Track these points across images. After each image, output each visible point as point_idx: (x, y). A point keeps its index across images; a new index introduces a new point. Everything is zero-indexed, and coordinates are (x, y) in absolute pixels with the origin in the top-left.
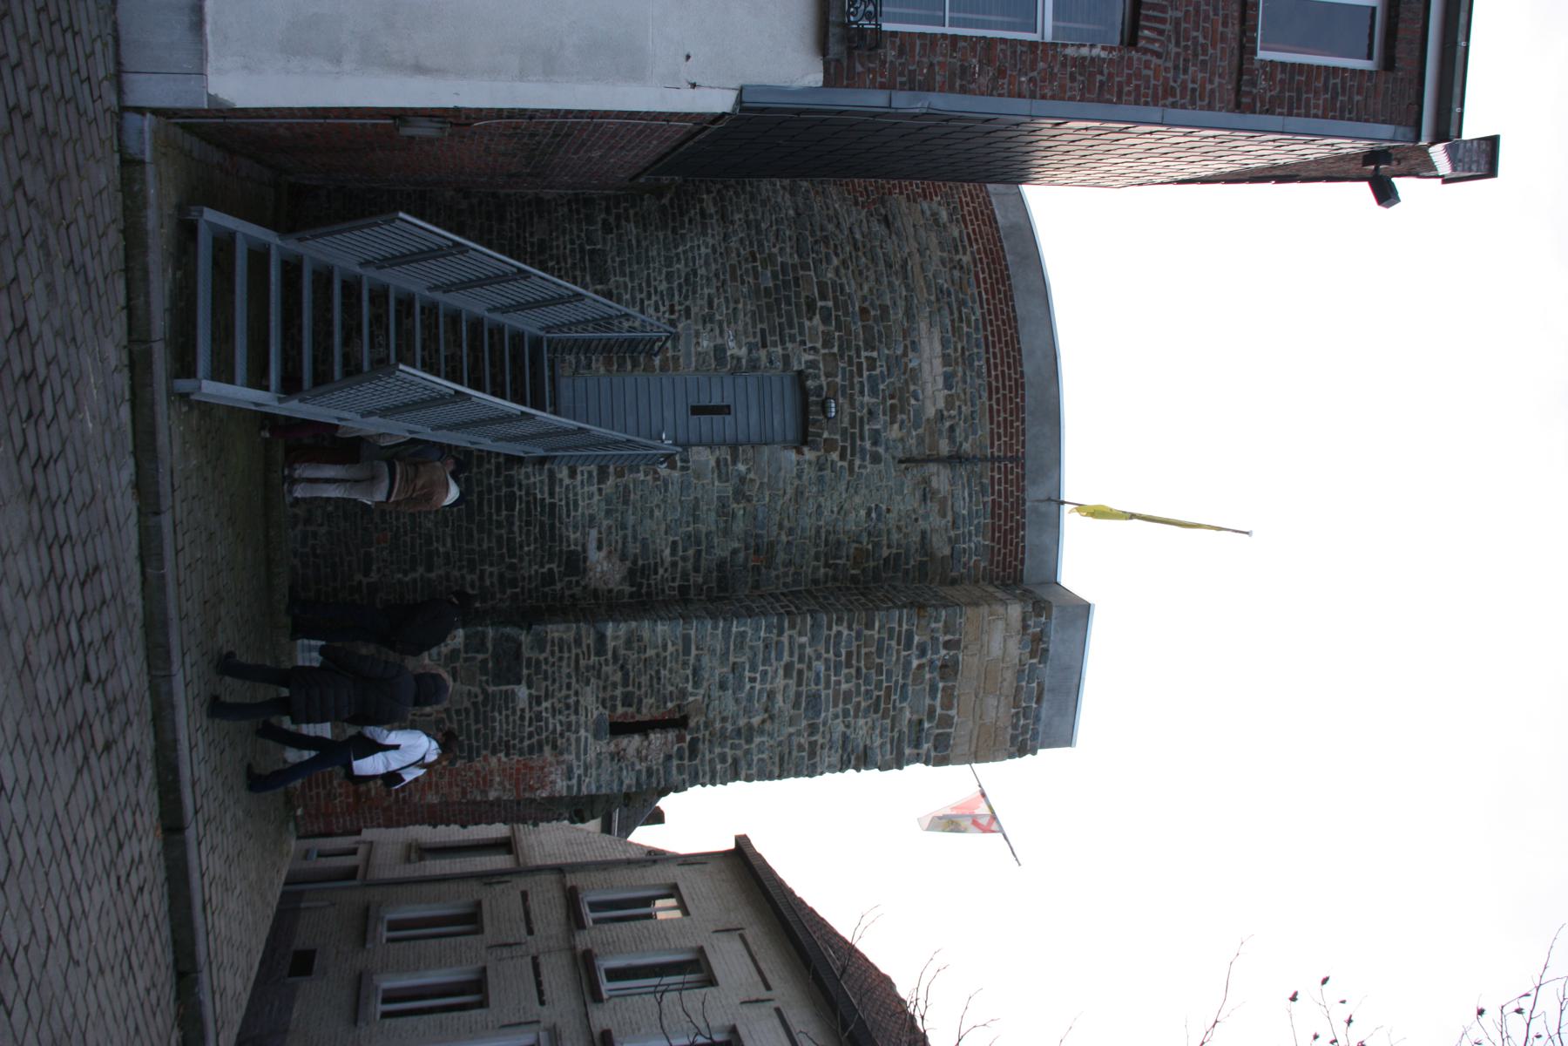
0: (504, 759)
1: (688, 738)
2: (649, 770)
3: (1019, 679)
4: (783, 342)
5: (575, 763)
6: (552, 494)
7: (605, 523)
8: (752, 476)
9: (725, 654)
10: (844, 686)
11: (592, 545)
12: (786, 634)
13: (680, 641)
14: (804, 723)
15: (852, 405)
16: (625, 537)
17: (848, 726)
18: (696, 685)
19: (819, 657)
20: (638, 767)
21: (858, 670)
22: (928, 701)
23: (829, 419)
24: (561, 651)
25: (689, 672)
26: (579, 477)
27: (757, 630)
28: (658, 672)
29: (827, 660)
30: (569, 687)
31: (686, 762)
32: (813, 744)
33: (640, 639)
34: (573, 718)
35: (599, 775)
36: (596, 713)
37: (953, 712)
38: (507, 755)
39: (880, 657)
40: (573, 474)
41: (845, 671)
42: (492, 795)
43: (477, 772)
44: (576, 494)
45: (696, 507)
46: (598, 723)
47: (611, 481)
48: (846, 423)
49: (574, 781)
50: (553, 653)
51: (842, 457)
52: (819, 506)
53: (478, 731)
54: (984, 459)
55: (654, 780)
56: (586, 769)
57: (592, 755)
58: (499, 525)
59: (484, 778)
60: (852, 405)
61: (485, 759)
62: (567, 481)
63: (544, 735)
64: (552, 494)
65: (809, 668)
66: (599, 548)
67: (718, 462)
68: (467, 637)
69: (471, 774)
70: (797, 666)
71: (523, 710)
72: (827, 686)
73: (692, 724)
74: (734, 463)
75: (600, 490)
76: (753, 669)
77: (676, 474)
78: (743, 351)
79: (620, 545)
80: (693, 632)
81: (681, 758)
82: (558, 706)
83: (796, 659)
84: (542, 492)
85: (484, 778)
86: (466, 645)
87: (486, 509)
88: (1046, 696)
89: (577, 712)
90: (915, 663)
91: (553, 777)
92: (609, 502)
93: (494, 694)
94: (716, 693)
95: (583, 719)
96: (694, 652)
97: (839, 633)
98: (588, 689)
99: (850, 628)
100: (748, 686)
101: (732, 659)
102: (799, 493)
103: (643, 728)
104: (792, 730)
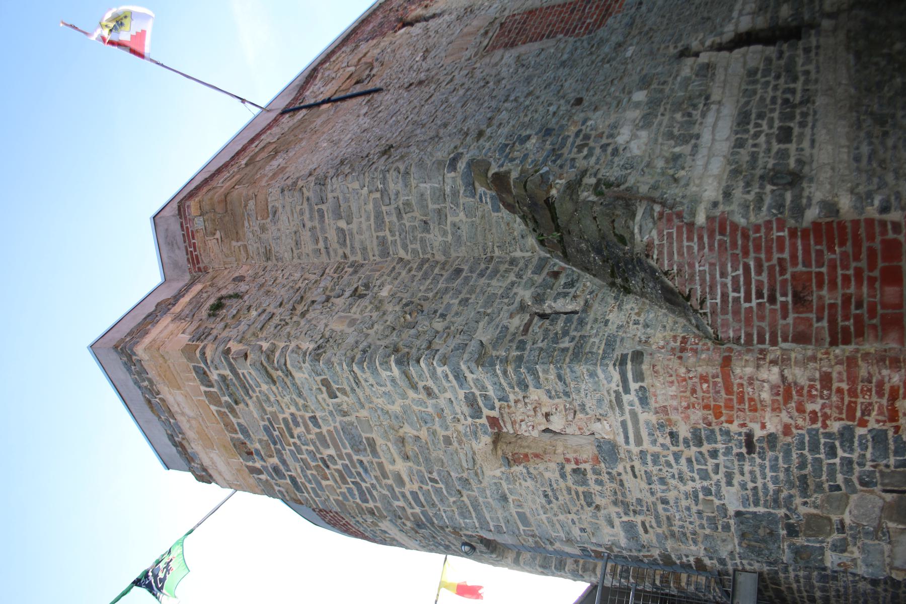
49: (634, 386)
69: (810, 407)
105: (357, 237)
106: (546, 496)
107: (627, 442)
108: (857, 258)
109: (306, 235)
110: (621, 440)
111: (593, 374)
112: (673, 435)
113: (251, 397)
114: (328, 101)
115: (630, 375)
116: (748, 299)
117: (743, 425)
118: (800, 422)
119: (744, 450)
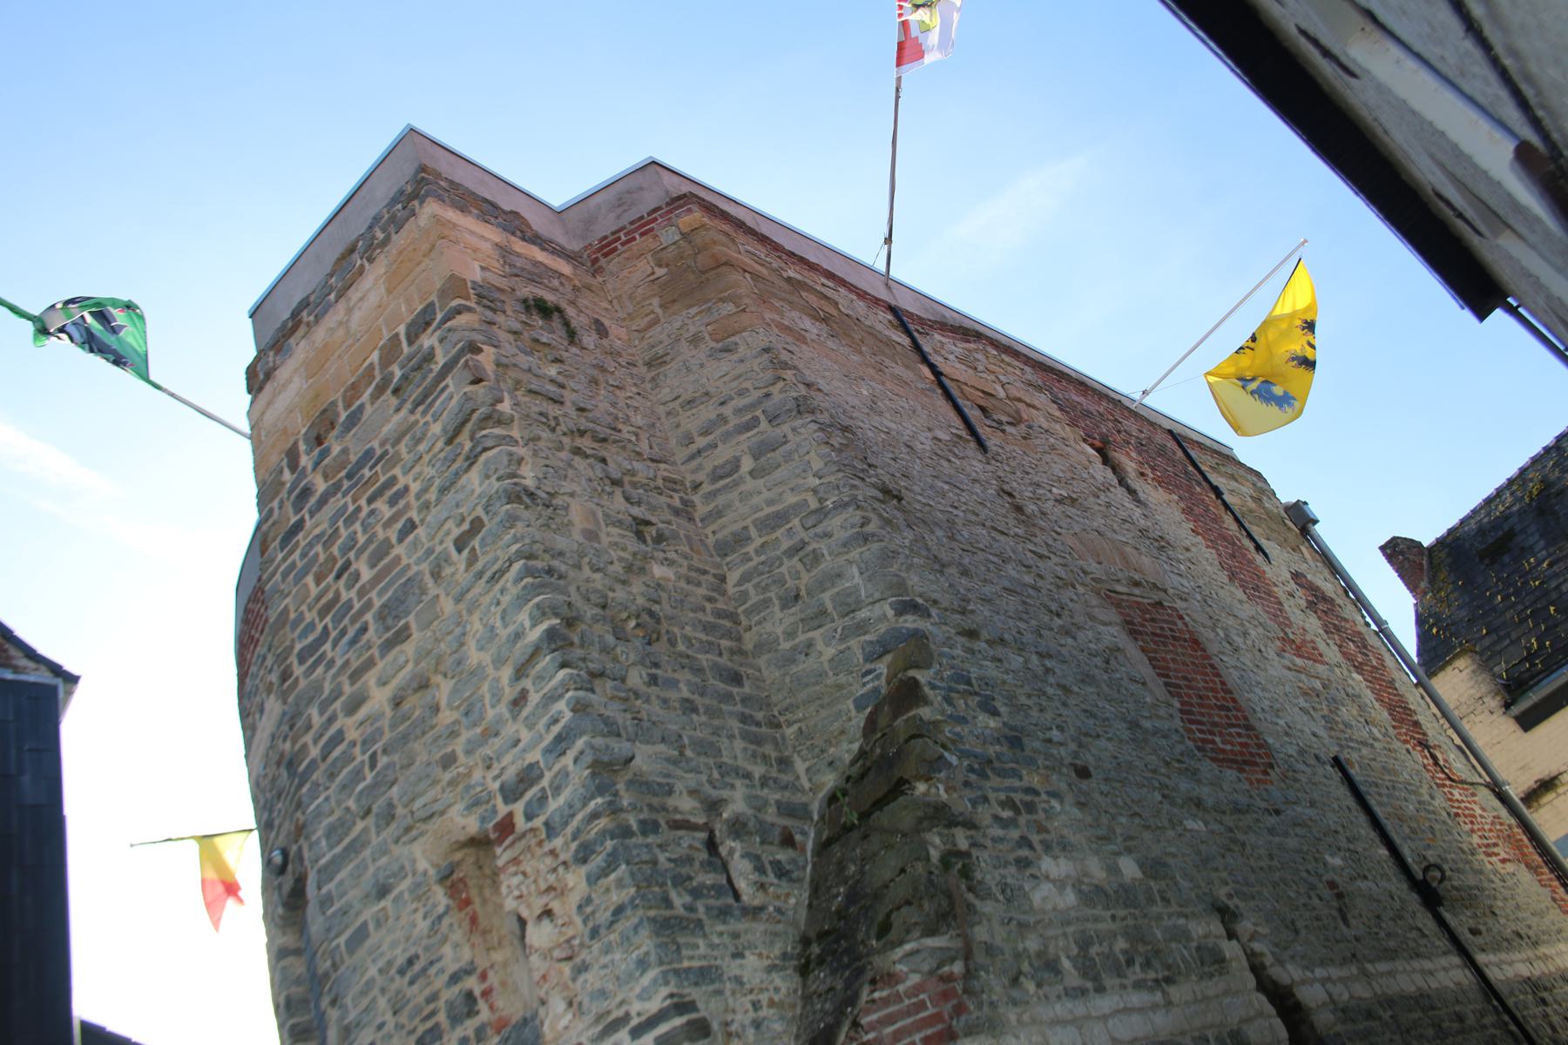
105: (734, 495)
109: (708, 412)
111: (643, 964)
113: (412, 412)
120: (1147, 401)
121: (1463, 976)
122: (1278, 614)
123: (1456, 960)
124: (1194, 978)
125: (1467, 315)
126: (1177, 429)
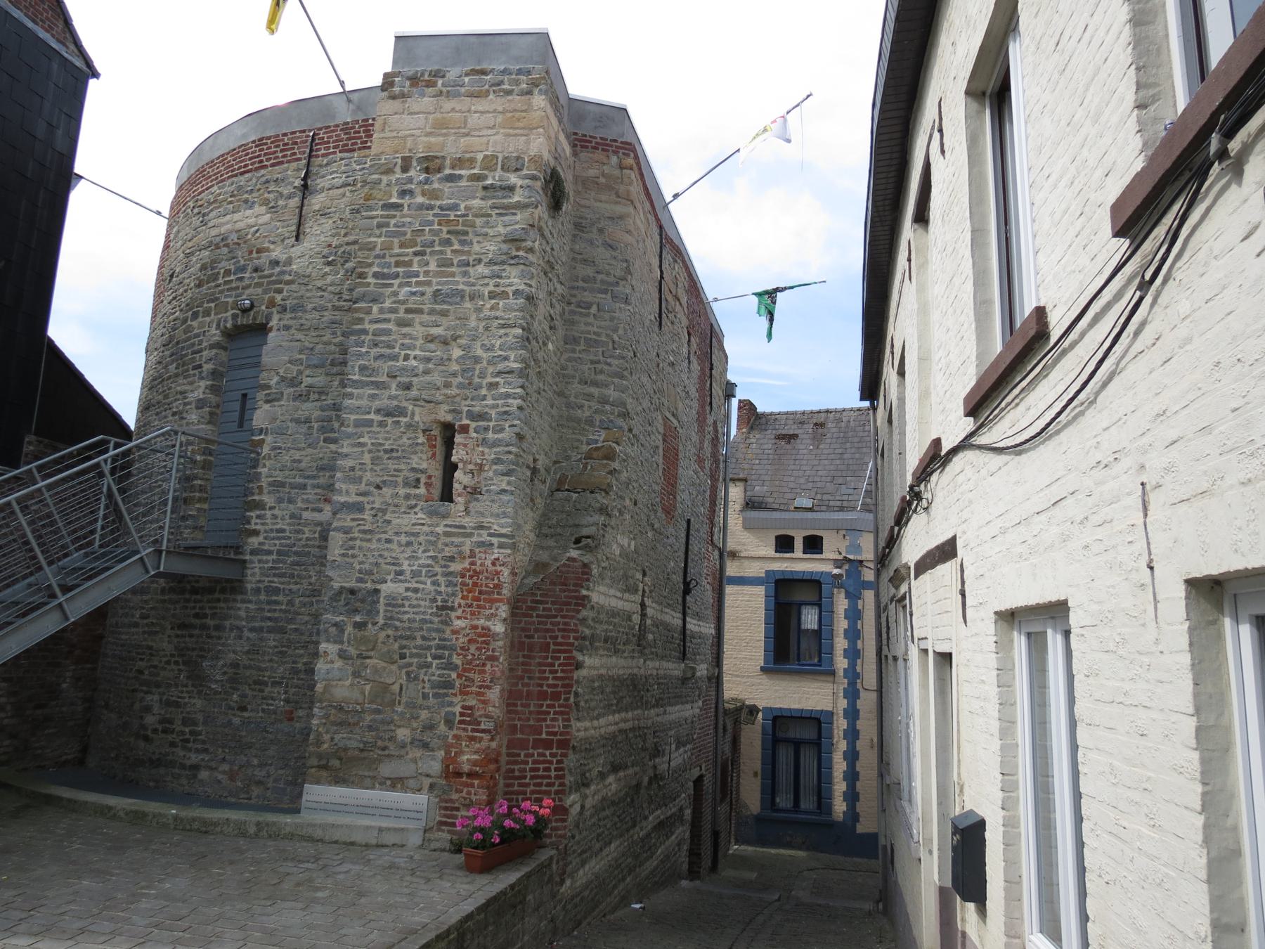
0: (459, 612)
1: (465, 422)
2: (498, 461)
3: (459, 95)
4: (200, 351)
5: (474, 539)
6: (269, 553)
7: (300, 505)
8: (281, 372)
9: (377, 385)
10: (433, 266)
11: (317, 516)
12: (367, 326)
13: (360, 430)
14: (468, 305)
15: (248, 286)
16: (314, 487)
17: (480, 261)
18: (402, 412)
19: (395, 294)
20: (491, 474)
21: (416, 254)
22: (464, 183)
23: (252, 306)
24: (352, 548)
25: (390, 420)
26: (258, 527)
27: (360, 355)
28: (386, 451)
29: (401, 285)
30: (388, 541)
31: (491, 424)
32: (492, 295)
33: (352, 469)
34: (422, 538)
35: (492, 515)
36: (420, 515)
37: (480, 157)
38: (452, 609)
39: (405, 234)
40: (256, 533)
41: (415, 268)
42: (499, 628)
43: (470, 641)
44: (272, 530)
45: (298, 421)
46: (431, 514)
47: (265, 498)
48: (259, 290)
49: (495, 540)
50: (354, 556)
51: (280, 291)
52: (315, 309)
53: (424, 638)
54: (308, 165)
55: (504, 457)
56: (482, 527)
57: (468, 522)
58: (290, 603)
59: (480, 635)
60: (248, 286)
61: (454, 632)
62: (261, 539)
63: (438, 569)
64: (269, 553)
65: (404, 302)
66: (320, 511)
67: (267, 402)
68: (328, 641)
69: (473, 648)
70: (401, 314)
71: (407, 589)
72: (429, 283)
73: (449, 418)
74: (269, 387)
75: (271, 508)
76: (395, 358)
77: (269, 439)
78: (203, 384)
79: (319, 491)
80: (353, 417)
81: (486, 429)
82: (408, 554)
83: (393, 316)
84: (267, 562)
85: (480, 635)
86: (335, 642)
87: (276, 615)
88: (485, 66)
89: (416, 535)
90: (420, 199)
91: (488, 563)
92: (280, 500)
93: (386, 618)
94: (414, 393)
95: (425, 528)
96: (372, 416)
97: (376, 275)
98: (395, 522)
99: (370, 265)
100: (414, 363)
101: (384, 379)
102: (301, 328)
103: (450, 469)
104: (474, 317)
105: (583, 319)
106: (392, 450)
107: (446, 526)
108: (554, 678)
109: (590, 271)
110: (449, 522)
111: (505, 515)
112: (452, 559)
113: (492, 208)
114: (662, 277)
115: (503, 540)
116: (538, 616)
117: (460, 606)
118: (461, 640)
119: (439, 603)
120: (714, 305)
121: (680, 622)
122: (702, 442)
123: (680, 615)
124: (608, 581)
125: (858, 394)
126: (715, 326)
